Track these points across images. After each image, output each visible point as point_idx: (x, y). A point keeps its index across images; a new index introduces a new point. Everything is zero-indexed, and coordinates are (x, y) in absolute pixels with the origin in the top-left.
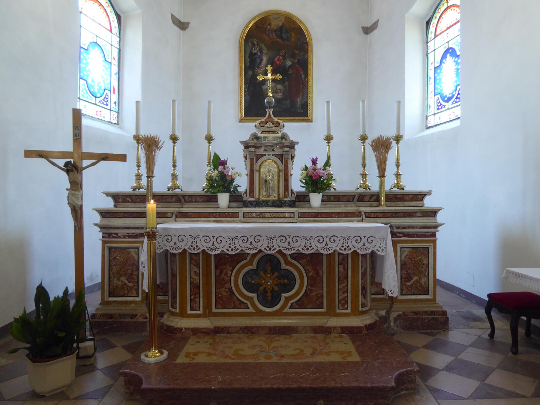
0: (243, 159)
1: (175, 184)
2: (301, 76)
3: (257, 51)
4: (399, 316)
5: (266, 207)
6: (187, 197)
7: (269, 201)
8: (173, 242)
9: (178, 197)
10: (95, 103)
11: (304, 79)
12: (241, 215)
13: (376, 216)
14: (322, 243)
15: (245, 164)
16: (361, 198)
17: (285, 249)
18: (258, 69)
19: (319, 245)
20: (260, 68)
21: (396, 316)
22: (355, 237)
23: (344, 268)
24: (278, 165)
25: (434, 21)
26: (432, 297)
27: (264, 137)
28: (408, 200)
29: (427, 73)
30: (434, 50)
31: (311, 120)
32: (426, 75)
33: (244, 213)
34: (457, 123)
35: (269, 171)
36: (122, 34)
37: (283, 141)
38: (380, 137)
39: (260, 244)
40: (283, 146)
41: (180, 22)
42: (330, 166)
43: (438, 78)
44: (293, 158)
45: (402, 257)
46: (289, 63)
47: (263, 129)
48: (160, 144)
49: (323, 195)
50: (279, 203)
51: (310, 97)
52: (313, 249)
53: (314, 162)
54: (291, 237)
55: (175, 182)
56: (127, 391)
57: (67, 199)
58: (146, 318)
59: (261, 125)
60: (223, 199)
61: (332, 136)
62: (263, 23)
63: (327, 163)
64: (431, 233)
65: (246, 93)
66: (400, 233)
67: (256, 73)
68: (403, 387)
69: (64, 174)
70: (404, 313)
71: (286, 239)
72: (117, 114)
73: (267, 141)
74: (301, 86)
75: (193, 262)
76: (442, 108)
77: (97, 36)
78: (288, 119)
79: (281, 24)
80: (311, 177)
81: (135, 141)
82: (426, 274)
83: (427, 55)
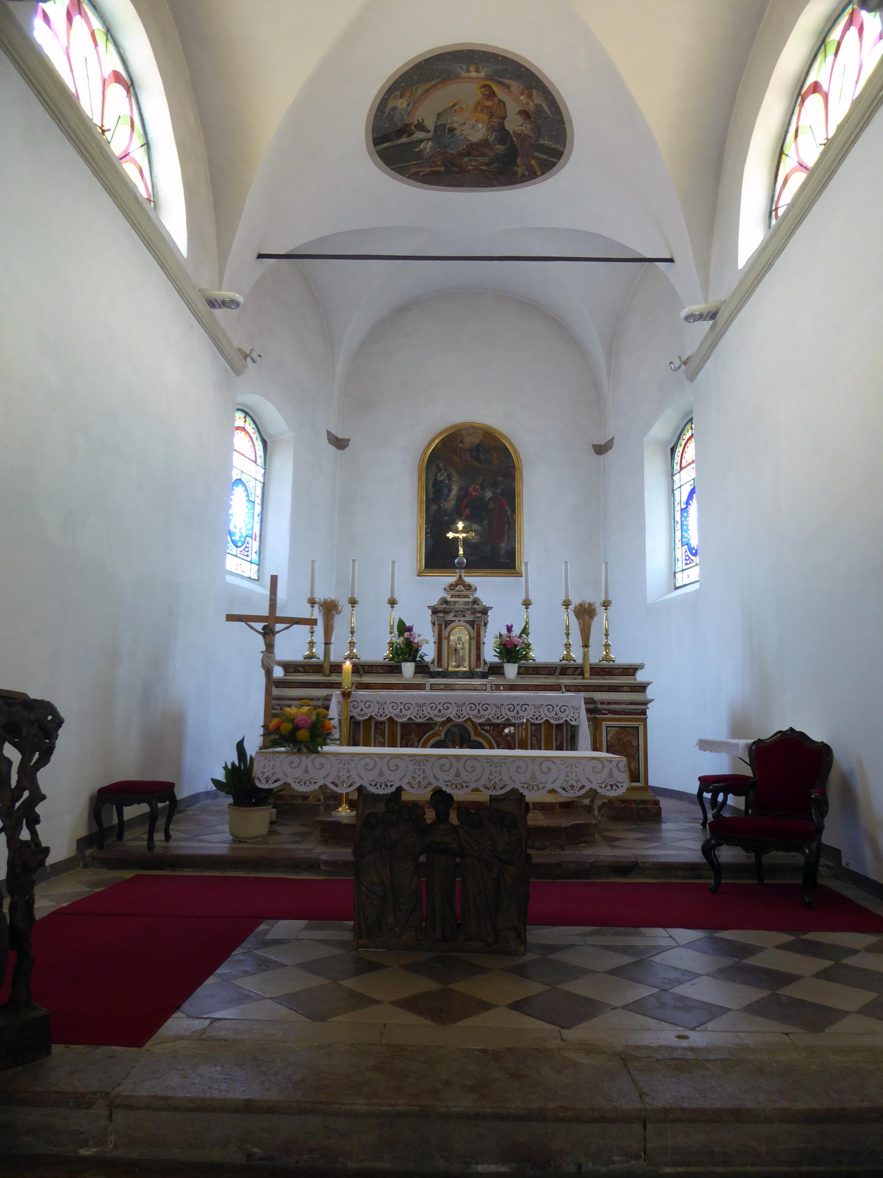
0: (430, 625)
1: (353, 653)
2: (506, 511)
3: (445, 478)
4: (604, 804)
5: (455, 678)
6: (366, 667)
7: (459, 672)
8: (359, 709)
9: (357, 668)
10: (235, 554)
11: (510, 516)
12: (428, 687)
13: (577, 690)
14: (513, 711)
15: (433, 631)
16: (564, 670)
17: (475, 717)
18: (446, 503)
19: (510, 714)
20: (448, 501)
21: (600, 804)
22: (547, 705)
23: (537, 740)
24: (468, 632)
25: (679, 449)
26: (643, 785)
27: (454, 601)
28: (618, 674)
29: (674, 515)
30: (680, 487)
31: (521, 574)
32: (673, 518)
33: (431, 684)
34: (697, 586)
35: (460, 639)
36: (267, 463)
37: (475, 606)
38: (582, 602)
39: (448, 711)
40: (474, 612)
41: (337, 438)
42: (527, 635)
43: (685, 523)
44: (486, 624)
45: (608, 737)
46: (489, 495)
47: (453, 592)
48: (340, 608)
49: (519, 667)
50: (471, 675)
51: (520, 541)
52: (504, 717)
53: (509, 629)
54: (481, 705)
55: (352, 651)
56: (322, 839)
57: (261, 661)
58: (319, 800)
59: (452, 588)
60: (408, 668)
61: (530, 600)
62: (453, 439)
63: (525, 631)
64: (641, 711)
65: (428, 536)
66: (605, 710)
67: (442, 508)
68: (582, 840)
69: (261, 637)
70: (609, 801)
71: (476, 707)
72: (257, 567)
73: (457, 606)
74: (506, 526)
75: (379, 731)
76: (690, 563)
77: (242, 472)
78: (487, 573)
79: (477, 441)
80: (505, 645)
81: (310, 605)
82: (636, 758)
83: (673, 491)
